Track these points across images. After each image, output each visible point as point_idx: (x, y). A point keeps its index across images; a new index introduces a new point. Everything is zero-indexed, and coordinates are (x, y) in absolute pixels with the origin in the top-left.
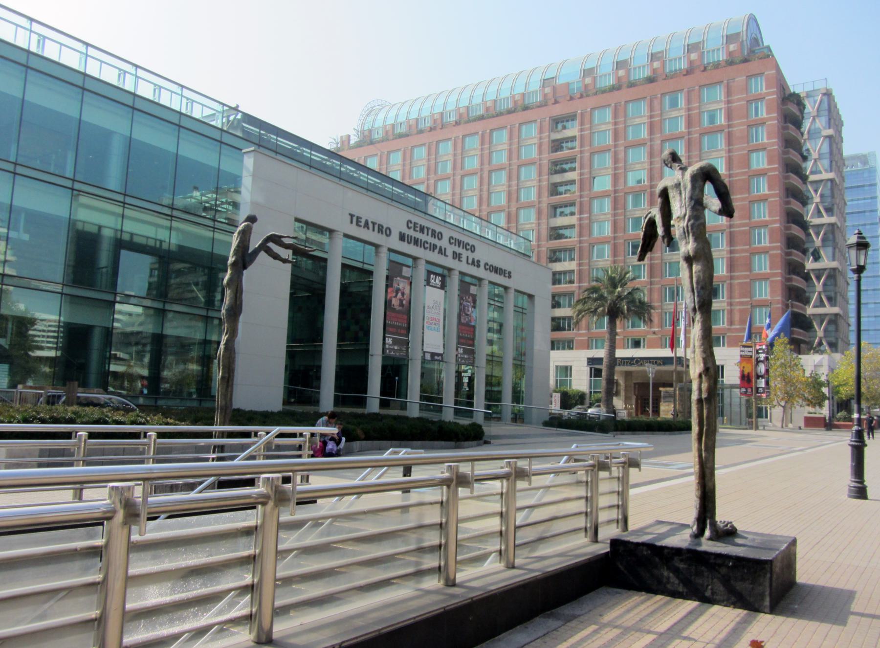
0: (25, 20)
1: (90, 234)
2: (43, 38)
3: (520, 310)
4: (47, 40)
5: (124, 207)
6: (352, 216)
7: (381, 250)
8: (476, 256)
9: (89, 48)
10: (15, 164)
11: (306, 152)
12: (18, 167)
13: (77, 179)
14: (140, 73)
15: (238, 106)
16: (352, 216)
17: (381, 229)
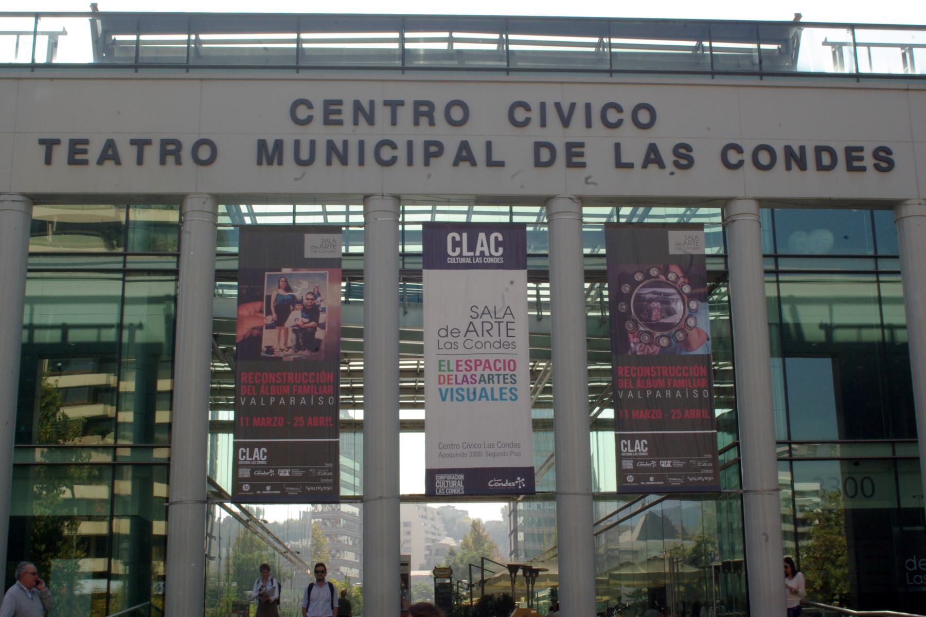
0: (844, 31)
1: (107, 344)
2: (908, 49)
3: (884, 265)
4: (915, 50)
5: (878, 282)
6: (49, 144)
7: (737, 207)
8: (665, 137)
9: (857, 31)
10: (876, 257)
11: (317, 41)
12: (880, 261)
13: (880, 253)
14: (862, 35)
15: (798, 16)
16: (49, 144)
17: (170, 150)
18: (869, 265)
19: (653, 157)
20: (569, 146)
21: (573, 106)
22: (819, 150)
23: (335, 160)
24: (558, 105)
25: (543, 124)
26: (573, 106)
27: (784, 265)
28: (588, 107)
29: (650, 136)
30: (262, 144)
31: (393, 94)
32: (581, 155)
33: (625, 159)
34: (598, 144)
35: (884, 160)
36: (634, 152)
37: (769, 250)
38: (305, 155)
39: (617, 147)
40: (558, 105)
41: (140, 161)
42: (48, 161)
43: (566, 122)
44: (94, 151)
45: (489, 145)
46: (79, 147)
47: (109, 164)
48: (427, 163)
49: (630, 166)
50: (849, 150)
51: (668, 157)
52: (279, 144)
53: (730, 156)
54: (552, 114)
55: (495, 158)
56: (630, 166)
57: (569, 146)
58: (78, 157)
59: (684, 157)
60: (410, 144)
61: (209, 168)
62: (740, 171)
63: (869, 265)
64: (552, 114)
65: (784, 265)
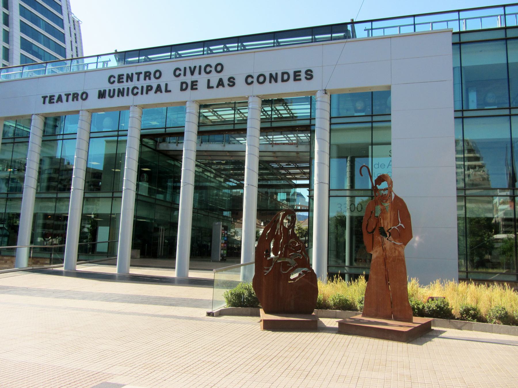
6: (45, 98)
8: (225, 76)
17: (75, 96)
18: (507, 112)
19: (221, 83)
20: (192, 82)
21: (195, 67)
22: (283, 74)
23: (273, 81)
24: (190, 68)
25: (185, 75)
26: (195, 67)
27: (466, 114)
28: (200, 67)
29: (220, 75)
30: (100, 92)
31: (138, 71)
32: (196, 85)
33: (211, 85)
34: (202, 79)
35: (309, 75)
36: (214, 83)
37: (459, 108)
38: (112, 94)
39: (209, 81)
40: (190, 68)
41: (67, 101)
42: (44, 103)
43: (192, 73)
44: (56, 98)
45: (166, 85)
46: (297, 74)
47: (221, 87)
48: (147, 93)
49: (212, 87)
50: (295, 72)
51: (226, 82)
52: (105, 91)
53: (248, 80)
54: (188, 71)
55: (169, 89)
56: (212, 87)
57: (192, 82)
58: (297, 78)
59: (232, 82)
60: (142, 87)
61: (246, 85)
62: (251, 86)
63: (507, 112)
64: (188, 71)
65: (466, 114)
